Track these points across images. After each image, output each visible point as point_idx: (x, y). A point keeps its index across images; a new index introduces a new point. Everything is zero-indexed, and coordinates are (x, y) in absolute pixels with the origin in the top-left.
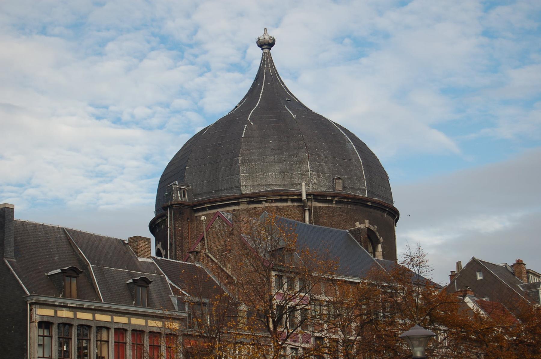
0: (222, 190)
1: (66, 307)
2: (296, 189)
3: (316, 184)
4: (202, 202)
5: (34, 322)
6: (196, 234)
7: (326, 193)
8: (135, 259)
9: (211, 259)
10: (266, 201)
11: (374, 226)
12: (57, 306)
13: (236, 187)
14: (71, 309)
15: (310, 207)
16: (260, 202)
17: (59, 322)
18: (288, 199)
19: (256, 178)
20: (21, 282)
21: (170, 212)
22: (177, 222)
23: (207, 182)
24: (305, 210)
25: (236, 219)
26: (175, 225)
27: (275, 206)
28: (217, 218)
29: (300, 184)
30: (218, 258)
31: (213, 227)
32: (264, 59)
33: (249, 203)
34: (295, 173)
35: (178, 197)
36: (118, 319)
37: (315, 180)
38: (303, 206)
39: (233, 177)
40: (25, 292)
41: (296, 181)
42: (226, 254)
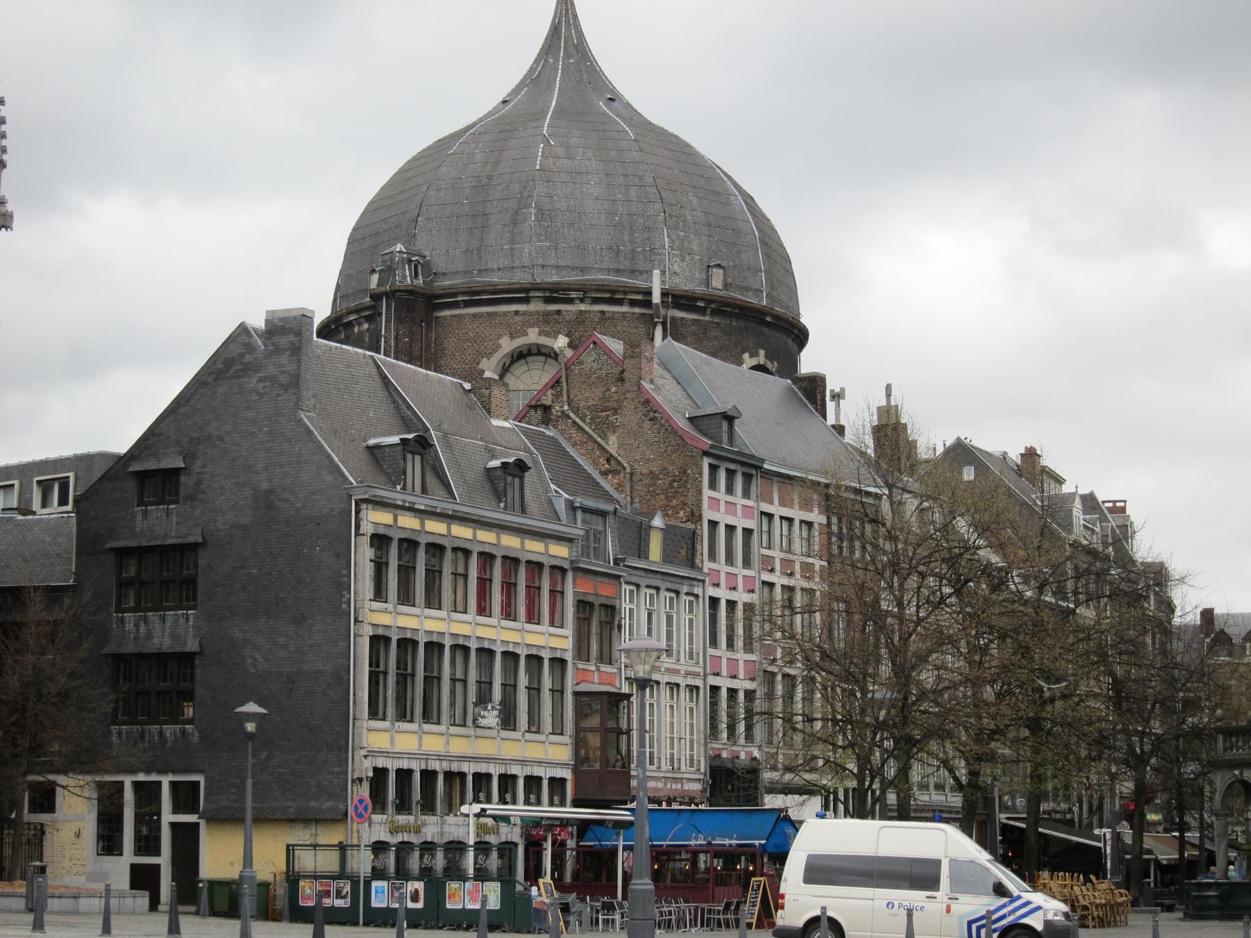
0: (492, 270)
1: (411, 509)
2: (639, 283)
3: (678, 275)
4: (453, 291)
5: (363, 535)
6: (436, 351)
7: (695, 293)
8: (487, 422)
9: (574, 422)
10: (582, 300)
11: (772, 363)
13: (524, 267)
14: (417, 515)
15: (665, 317)
16: (570, 301)
17: (455, 546)
18: (624, 299)
19: (564, 252)
21: (386, 305)
22: (401, 327)
23: (463, 252)
24: (655, 324)
25: (633, 352)
26: (397, 331)
27: (599, 312)
28: (592, 346)
29: (649, 273)
30: (591, 423)
31: (581, 363)
32: (561, 11)
33: (548, 300)
34: (639, 250)
35: (404, 277)
36: (486, 536)
37: (676, 267)
38: (651, 315)
39: (518, 246)
40: (346, 479)
41: (641, 265)
42: (608, 416)
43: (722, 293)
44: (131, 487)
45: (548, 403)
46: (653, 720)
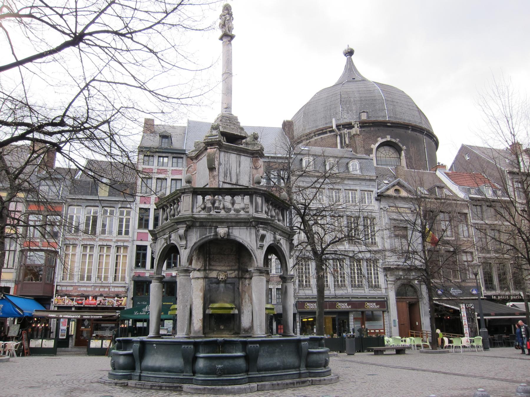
10: (315, 136)
46: (126, 263)
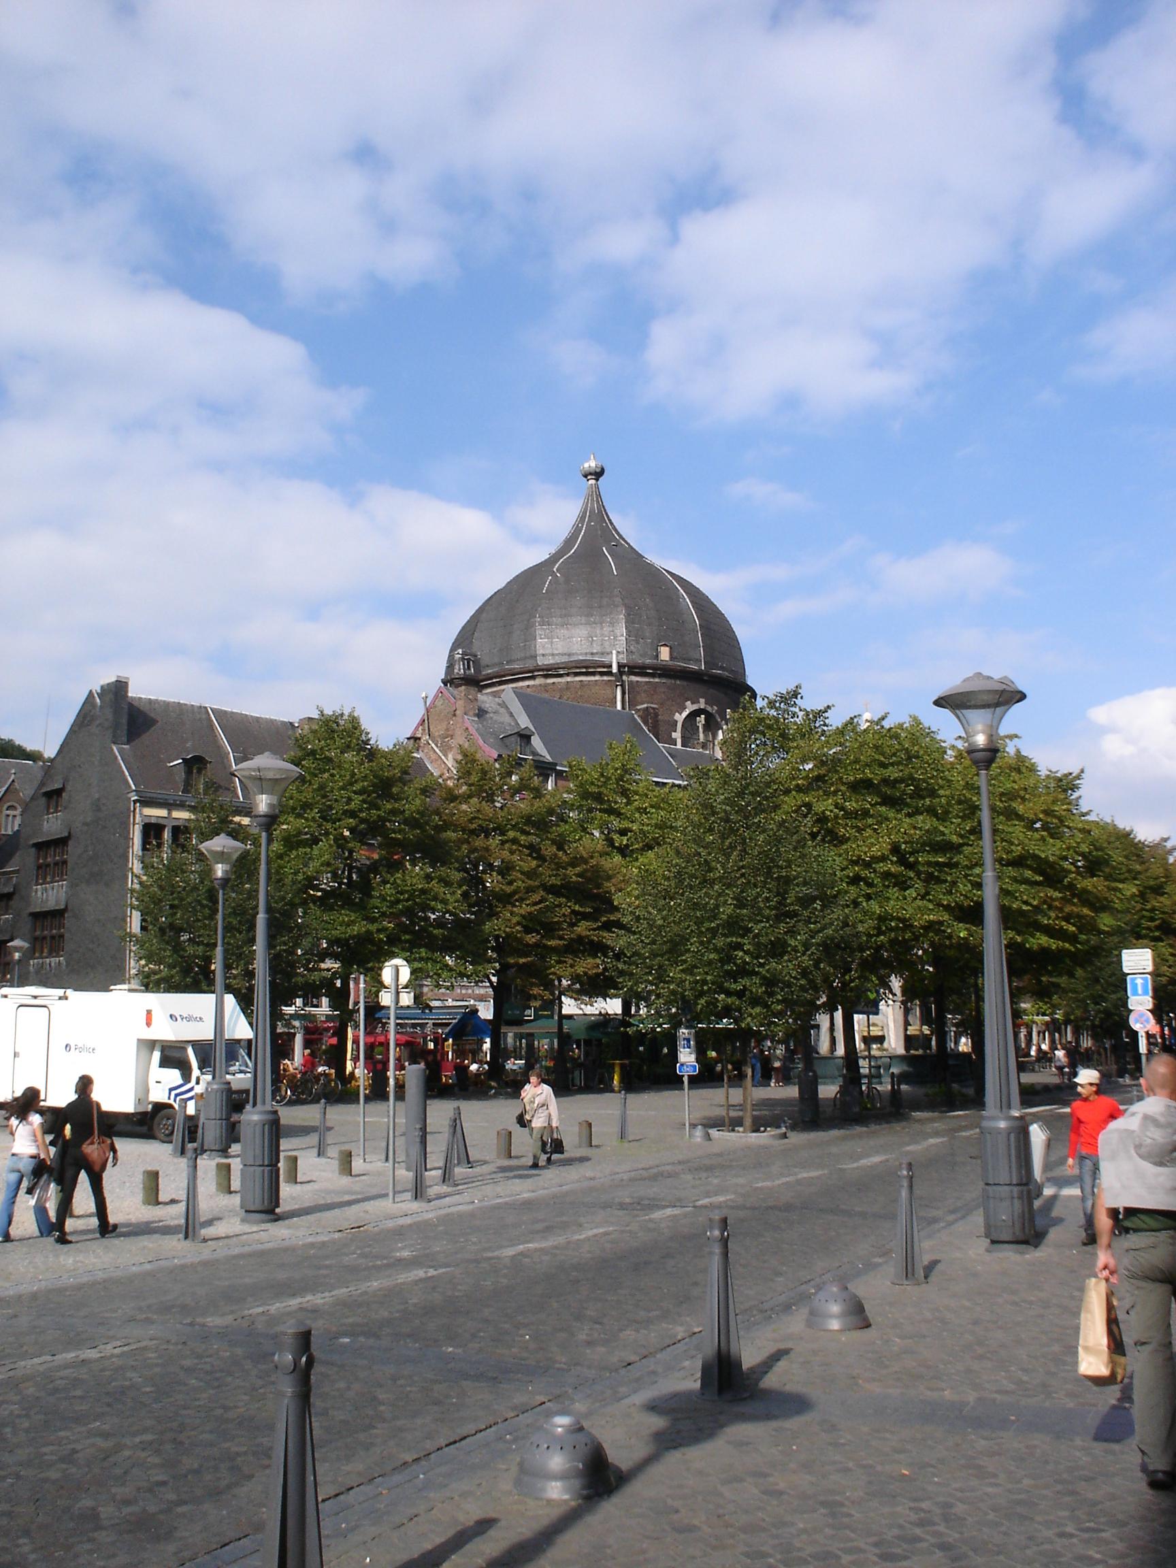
2: (605, 659)
12: (171, 805)
16: (561, 676)
20: (127, 774)
33: (546, 676)
43: (671, 663)
44: (43, 801)
45: (419, 736)
